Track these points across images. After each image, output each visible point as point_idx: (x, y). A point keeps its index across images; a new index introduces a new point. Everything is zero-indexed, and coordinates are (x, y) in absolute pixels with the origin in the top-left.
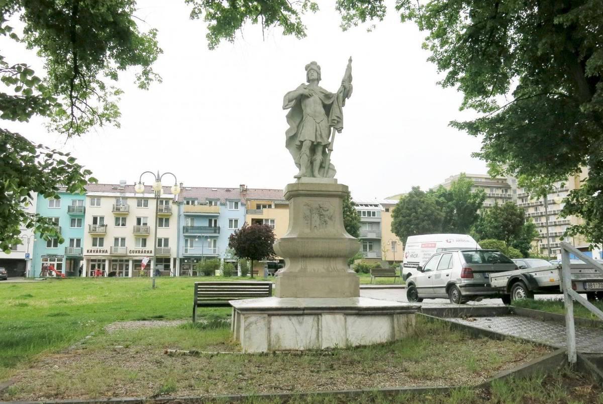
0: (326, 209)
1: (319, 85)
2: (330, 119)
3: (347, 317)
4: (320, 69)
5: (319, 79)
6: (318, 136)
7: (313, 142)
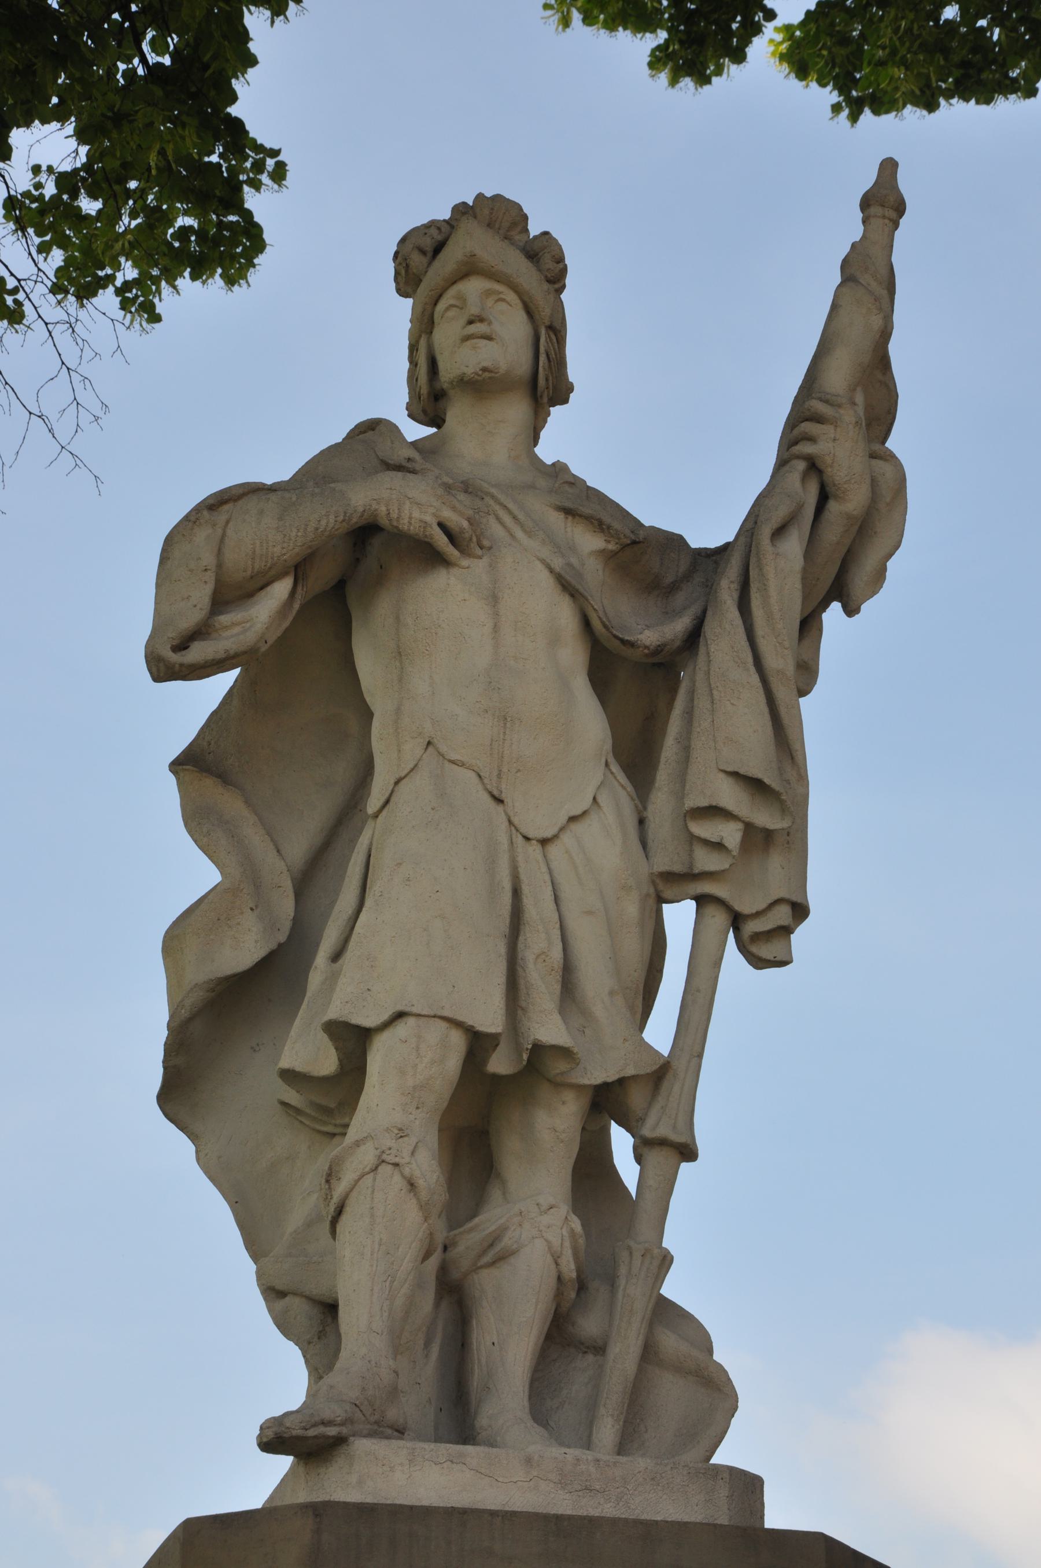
1: (547, 451)
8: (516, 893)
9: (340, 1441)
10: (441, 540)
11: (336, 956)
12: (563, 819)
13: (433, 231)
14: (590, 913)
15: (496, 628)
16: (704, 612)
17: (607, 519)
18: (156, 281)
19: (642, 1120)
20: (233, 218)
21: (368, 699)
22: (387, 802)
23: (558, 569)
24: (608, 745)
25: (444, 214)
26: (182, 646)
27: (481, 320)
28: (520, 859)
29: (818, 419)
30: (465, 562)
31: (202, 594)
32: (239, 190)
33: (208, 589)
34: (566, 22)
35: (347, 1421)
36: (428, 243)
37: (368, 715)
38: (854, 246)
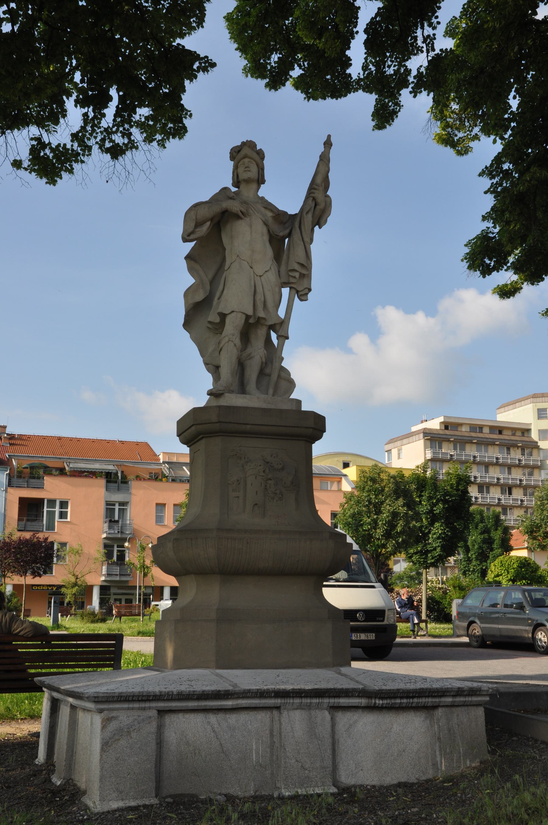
0: (280, 467)
1: (261, 193)
2: (283, 268)
3: (336, 714)
4: (263, 158)
5: (261, 180)
6: (260, 306)
7: (248, 317)
8: (255, 286)
9: (222, 394)
10: (240, 214)
11: (219, 299)
12: (264, 272)
13: (238, 148)
14: (269, 291)
15: (251, 232)
16: (292, 229)
17: (273, 210)
18: (165, 140)
19: (278, 331)
20: (181, 125)
21: (225, 246)
22: (229, 268)
23: (264, 220)
24: (273, 256)
25: (239, 144)
26: (189, 235)
27: (248, 167)
28: (256, 279)
29: (315, 189)
30: (245, 218)
31: (193, 225)
32: (182, 119)
33: (194, 223)
34: (247, 76)
35: (224, 390)
36: (237, 150)
37: (224, 249)
38: (322, 153)
